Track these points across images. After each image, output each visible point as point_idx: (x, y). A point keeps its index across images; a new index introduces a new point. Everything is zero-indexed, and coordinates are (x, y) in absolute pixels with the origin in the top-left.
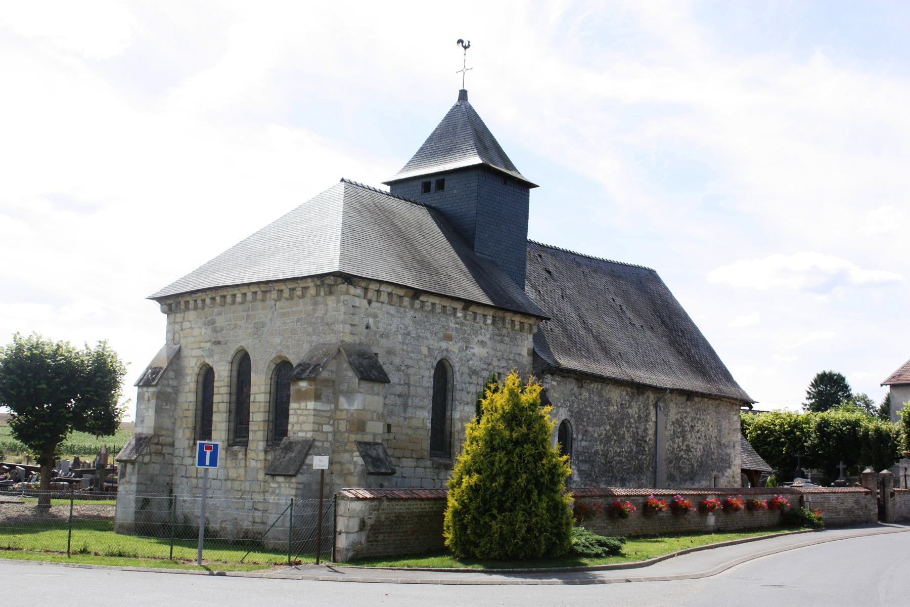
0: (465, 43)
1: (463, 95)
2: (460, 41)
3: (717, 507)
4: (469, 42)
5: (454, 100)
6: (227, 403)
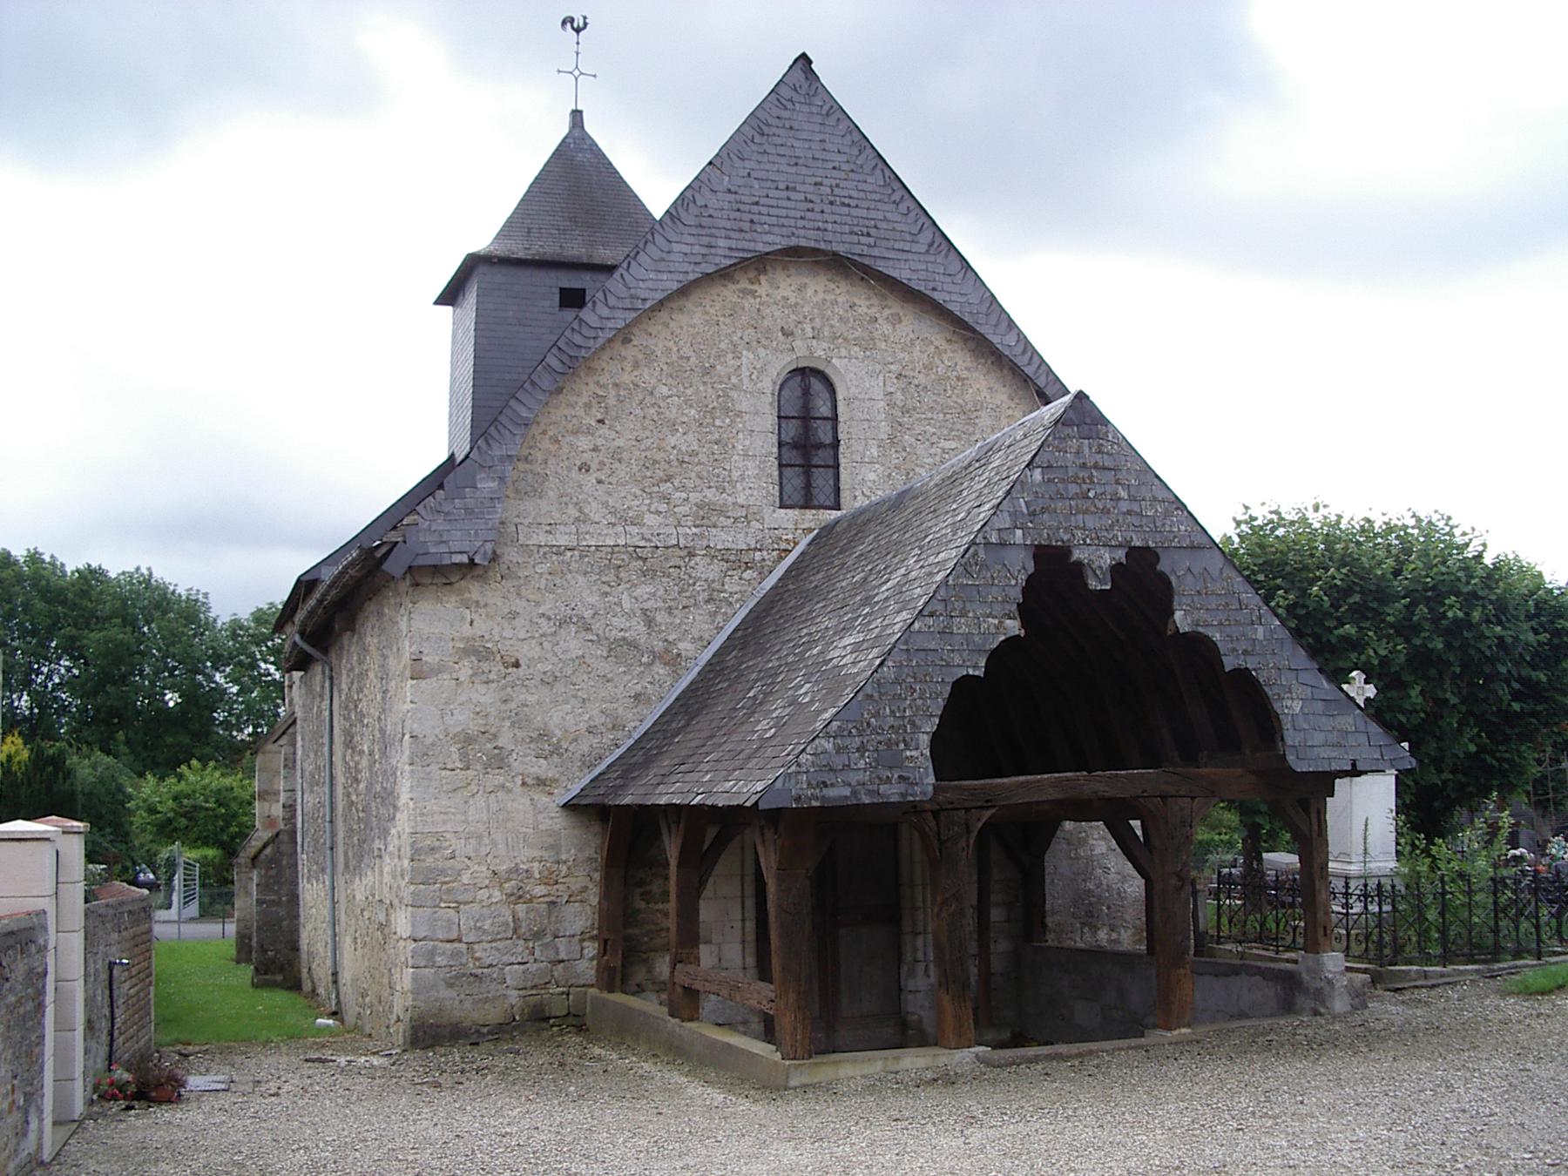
0: (579, 22)
1: (577, 115)
2: (568, 21)
3: (151, 1064)
4: (585, 18)
5: (563, 129)
6: (224, 923)
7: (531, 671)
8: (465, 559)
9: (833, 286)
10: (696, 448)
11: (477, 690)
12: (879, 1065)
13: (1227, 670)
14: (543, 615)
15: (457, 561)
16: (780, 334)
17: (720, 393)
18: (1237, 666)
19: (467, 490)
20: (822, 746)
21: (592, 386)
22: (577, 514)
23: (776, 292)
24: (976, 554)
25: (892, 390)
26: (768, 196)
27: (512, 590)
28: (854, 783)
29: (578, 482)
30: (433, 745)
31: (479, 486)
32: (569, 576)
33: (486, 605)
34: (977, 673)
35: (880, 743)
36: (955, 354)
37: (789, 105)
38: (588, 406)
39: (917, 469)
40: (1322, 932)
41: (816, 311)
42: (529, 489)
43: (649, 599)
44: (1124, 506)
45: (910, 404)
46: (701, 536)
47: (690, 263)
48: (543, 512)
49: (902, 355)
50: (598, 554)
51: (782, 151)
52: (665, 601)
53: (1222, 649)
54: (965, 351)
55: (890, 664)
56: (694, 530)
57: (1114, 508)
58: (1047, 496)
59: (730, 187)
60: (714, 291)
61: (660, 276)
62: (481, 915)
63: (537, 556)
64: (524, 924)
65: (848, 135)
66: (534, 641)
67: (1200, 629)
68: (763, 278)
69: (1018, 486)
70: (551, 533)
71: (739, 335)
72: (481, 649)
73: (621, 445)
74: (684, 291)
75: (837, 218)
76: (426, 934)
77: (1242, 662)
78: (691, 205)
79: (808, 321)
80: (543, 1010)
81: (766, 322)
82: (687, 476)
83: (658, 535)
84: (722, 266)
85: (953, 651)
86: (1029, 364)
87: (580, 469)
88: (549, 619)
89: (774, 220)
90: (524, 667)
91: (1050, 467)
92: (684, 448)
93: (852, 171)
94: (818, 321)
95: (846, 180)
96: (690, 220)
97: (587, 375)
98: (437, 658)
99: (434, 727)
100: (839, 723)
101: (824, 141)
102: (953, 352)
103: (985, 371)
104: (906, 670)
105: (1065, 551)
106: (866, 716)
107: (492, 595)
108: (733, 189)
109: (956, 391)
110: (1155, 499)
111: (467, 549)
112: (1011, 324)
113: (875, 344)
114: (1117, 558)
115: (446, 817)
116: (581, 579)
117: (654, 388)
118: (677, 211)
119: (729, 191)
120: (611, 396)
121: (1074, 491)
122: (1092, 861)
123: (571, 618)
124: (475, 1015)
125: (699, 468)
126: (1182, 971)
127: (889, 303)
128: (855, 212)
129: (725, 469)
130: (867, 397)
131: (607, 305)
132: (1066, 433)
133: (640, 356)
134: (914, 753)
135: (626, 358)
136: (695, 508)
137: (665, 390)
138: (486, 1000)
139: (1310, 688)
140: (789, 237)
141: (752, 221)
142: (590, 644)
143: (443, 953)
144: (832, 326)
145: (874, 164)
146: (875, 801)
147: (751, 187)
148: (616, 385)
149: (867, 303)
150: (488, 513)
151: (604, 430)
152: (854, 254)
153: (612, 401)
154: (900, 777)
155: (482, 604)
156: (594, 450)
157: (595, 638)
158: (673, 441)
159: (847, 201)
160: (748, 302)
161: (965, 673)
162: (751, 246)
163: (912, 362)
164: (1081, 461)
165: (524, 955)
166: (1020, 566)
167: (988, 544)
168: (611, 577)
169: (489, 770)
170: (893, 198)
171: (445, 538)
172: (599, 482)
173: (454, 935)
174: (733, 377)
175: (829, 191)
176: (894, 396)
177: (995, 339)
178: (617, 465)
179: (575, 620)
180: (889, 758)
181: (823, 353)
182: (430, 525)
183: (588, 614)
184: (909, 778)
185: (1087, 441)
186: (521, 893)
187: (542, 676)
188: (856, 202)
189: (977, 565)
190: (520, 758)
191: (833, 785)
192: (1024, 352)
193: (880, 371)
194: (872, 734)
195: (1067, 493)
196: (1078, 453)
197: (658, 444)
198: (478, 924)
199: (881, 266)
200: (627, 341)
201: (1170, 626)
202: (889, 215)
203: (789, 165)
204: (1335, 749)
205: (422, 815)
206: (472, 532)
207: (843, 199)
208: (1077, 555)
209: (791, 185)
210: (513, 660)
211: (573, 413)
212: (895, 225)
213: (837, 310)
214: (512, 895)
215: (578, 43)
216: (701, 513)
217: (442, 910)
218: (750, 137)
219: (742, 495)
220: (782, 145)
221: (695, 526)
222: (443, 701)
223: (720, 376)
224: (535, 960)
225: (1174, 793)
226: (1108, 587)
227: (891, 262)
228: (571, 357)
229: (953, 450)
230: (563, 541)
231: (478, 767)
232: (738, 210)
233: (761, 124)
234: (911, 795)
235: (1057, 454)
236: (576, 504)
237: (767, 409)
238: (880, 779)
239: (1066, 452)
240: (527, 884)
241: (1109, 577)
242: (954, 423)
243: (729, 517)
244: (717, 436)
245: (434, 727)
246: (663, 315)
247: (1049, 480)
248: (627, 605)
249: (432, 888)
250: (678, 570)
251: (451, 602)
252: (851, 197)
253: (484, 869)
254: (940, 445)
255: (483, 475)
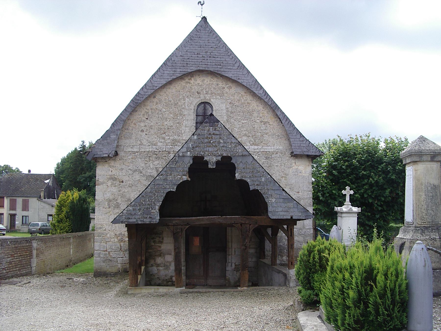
4: (204, 1)
7: (126, 183)
8: (107, 155)
9: (212, 79)
10: (172, 125)
11: (112, 188)
12: (153, 290)
13: (251, 190)
14: (130, 169)
15: (105, 156)
16: (196, 93)
17: (179, 110)
18: (254, 189)
19: (108, 138)
20: (129, 208)
21: (145, 110)
22: (140, 143)
23: (196, 82)
24: (175, 159)
25: (228, 107)
26: (192, 56)
27: (122, 163)
28: (137, 218)
29: (140, 135)
30: (101, 202)
31: (111, 137)
32: (137, 159)
33: (115, 167)
34: (173, 190)
35: (145, 208)
36: (247, 96)
37: (199, 31)
38: (144, 115)
39: (234, 129)
40: (291, 264)
41: (207, 87)
42: (128, 137)
43: (158, 165)
44: (221, 145)
45: (233, 111)
46: (172, 148)
47: (169, 76)
48: (131, 143)
49: (231, 97)
50: (144, 153)
51: (197, 44)
52: (162, 165)
53: (250, 184)
54: (250, 95)
55: (149, 188)
56: (171, 146)
57: (218, 146)
58: (198, 143)
59: (181, 55)
60: (179, 83)
61: (161, 80)
62: (112, 245)
63: (128, 154)
64: (123, 248)
65: (216, 38)
66: (127, 176)
67: (243, 179)
68: (192, 78)
69: (189, 140)
70: (132, 148)
71: (185, 94)
72: (114, 178)
73: (152, 125)
74: (170, 83)
75: (211, 61)
76: (98, 249)
77: (256, 187)
78: (170, 60)
79: (204, 89)
80: (127, 270)
81: (193, 90)
82: (170, 132)
83: (160, 148)
84: (178, 76)
85: (167, 184)
86: (266, 99)
87: (141, 131)
88: (131, 170)
89: (193, 63)
90: (124, 182)
91: (199, 135)
92: (169, 125)
93: (217, 48)
94: (207, 90)
95: (214, 50)
96: (170, 64)
97: (144, 107)
98: (103, 180)
99: (101, 197)
100: (134, 203)
101: (209, 40)
102: (246, 96)
103: (256, 101)
104: (153, 189)
105: (202, 157)
106: (141, 201)
107: (117, 164)
108: (182, 55)
109: (247, 107)
110: (232, 142)
111: (107, 153)
112: (261, 87)
113: (224, 95)
114: (218, 159)
115: (104, 220)
116: (140, 160)
117: (162, 109)
118: (166, 63)
119: (181, 56)
120: (150, 112)
121: (206, 141)
122: (282, 237)
123: (137, 170)
124: (110, 270)
125: (173, 130)
126: (245, 272)
127: (228, 83)
128: (216, 59)
129: (180, 130)
130: (221, 109)
131: (146, 88)
132: (205, 125)
133: (158, 101)
134: (154, 211)
135: (154, 102)
136: (171, 141)
137: (164, 110)
138: (113, 266)
139: (279, 195)
140: (197, 67)
141: (187, 64)
142: (141, 177)
143: (102, 254)
144: (211, 90)
145: (223, 45)
146: (142, 223)
147: (187, 54)
148: (151, 109)
149: (222, 83)
150: (113, 144)
151: (148, 121)
152: (216, 71)
153: (150, 113)
154: (149, 217)
155: (114, 166)
156: (145, 126)
157: (143, 175)
158: (166, 123)
159: (214, 56)
160: (188, 85)
161: (170, 190)
162: (186, 70)
163: (234, 99)
164: (209, 133)
165: (123, 255)
166: (188, 162)
167: (179, 156)
168: (148, 159)
169: (115, 208)
170: (228, 54)
171: (102, 150)
172: (146, 134)
173: (105, 250)
174: (183, 106)
175: (209, 53)
176: (229, 109)
177: (256, 92)
178: (151, 130)
179: (138, 170)
180: (147, 212)
181: (208, 98)
182: (98, 147)
183: (141, 169)
184: (152, 217)
185: (211, 127)
186: (122, 240)
187: (129, 185)
188: (217, 56)
189: (175, 161)
190: (123, 206)
191: (131, 219)
192: (265, 95)
193: (225, 102)
194: (143, 206)
195: (204, 142)
196: (208, 130)
197: (162, 124)
198: (111, 247)
199: (223, 74)
200: (154, 97)
201: (235, 179)
202: (227, 59)
203: (199, 47)
204: (285, 212)
205: (98, 219)
206: (109, 149)
207: (213, 56)
208: (205, 158)
209: (198, 53)
210: (122, 181)
211: (140, 117)
212: (228, 62)
213: (213, 86)
214: (120, 240)
215: (202, 8)
216: (173, 142)
217: (102, 243)
218: (188, 41)
219: (184, 137)
220: (197, 42)
221: (171, 146)
222: (104, 191)
223: (179, 106)
224: (125, 257)
225: (244, 223)
226: (214, 167)
227: (226, 72)
228: (136, 103)
229: (245, 123)
230: (135, 150)
231: (112, 208)
232: (183, 61)
233: (191, 37)
234: (153, 222)
235: (202, 131)
236: (140, 140)
237: (192, 114)
238: (144, 217)
239: (205, 130)
240: (124, 237)
241: (215, 164)
242: (246, 115)
243: (181, 143)
244: (178, 121)
245: (101, 197)
246: (165, 90)
247: (199, 138)
248: (152, 166)
249: (100, 238)
250: (165, 157)
251: (106, 166)
252: (216, 55)
253: (113, 233)
254: (242, 122)
255: (112, 134)
